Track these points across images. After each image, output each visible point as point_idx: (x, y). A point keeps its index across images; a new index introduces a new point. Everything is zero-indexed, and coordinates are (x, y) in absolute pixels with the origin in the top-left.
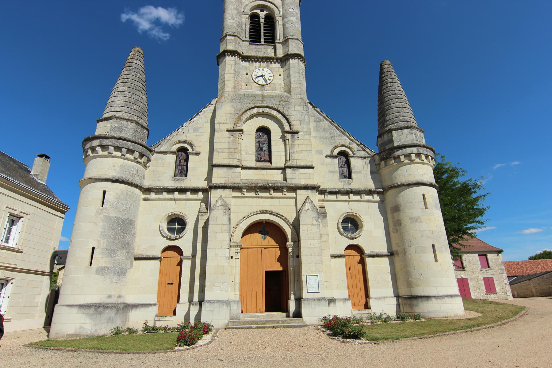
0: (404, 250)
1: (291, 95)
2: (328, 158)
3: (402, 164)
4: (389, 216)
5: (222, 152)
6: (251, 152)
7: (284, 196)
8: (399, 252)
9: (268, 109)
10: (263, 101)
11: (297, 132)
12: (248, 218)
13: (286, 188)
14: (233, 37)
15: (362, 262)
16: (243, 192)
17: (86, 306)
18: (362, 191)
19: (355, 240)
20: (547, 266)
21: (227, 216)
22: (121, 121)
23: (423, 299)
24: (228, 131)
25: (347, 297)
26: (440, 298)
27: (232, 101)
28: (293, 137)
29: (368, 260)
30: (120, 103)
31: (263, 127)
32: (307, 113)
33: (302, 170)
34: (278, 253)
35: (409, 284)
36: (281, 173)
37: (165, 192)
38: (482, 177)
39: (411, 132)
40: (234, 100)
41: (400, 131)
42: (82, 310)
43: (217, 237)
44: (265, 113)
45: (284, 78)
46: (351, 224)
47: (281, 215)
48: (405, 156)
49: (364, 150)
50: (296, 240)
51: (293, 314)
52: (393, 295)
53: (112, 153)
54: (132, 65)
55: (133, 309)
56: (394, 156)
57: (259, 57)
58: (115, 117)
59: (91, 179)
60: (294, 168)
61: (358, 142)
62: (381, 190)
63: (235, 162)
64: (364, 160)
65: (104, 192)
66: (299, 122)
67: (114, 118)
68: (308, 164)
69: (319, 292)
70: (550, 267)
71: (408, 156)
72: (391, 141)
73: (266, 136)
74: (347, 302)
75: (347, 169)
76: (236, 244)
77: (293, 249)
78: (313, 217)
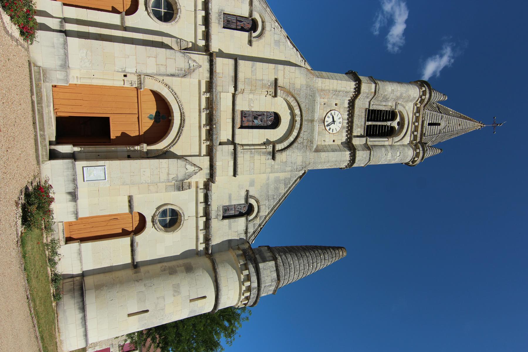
0: (140, 280)
2: (246, 193)
3: (239, 272)
4: (181, 262)
5: (252, 71)
6: (252, 105)
8: (138, 274)
9: (299, 126)
10: (308, 121)
11: (274, 158)
12: (175, 97)
13: (211, 144)
15: (125, 233)
21: (177, 72)
23: (81, 303)
26: (83, 323)
27: (308, 86)
28: (269, 153)
29: (127, 240)
33: (231, 163)
35: (98, 287)
36: (228, 140)
39: (274, 280)
40: (309, 89)
41: (275, 269)
43: (150, 58)
46: (170, 220)
47: (179, 138)
51: (54, 150)
52: (84, 270)
56: (248, 263)
57: (353, 119)
62: (210, 252)
63: (240, 86)
64: (243, 232)
68: (239, 170)
69: (84, 181)
72: (264, 260)
73: (270, 123)
74: (74, 215)
76: (142, 82)
77: (137, 152)
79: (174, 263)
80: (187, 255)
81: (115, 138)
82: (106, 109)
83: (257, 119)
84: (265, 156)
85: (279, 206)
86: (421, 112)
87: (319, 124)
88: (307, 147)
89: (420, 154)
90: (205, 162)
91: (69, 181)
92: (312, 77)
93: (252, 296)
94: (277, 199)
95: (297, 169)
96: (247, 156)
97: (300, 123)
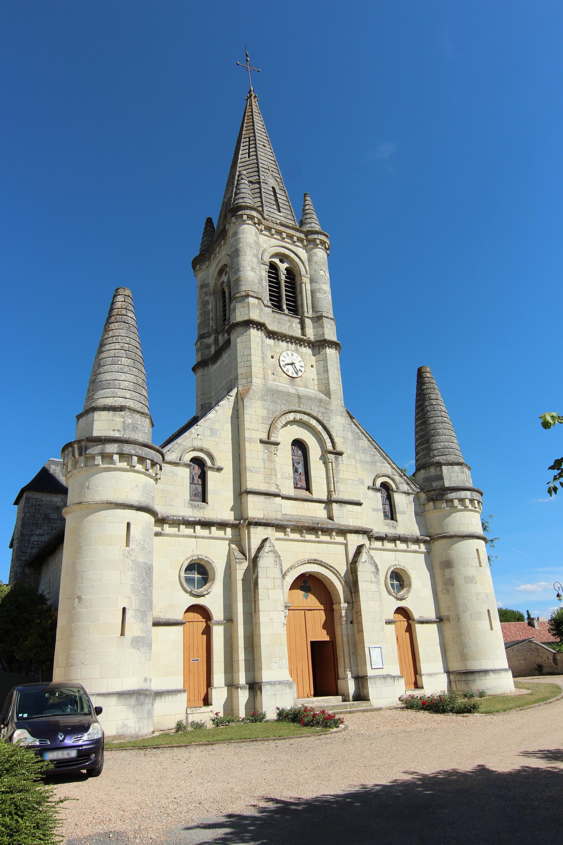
0: (458, 616)
1: (330, 399)
2: (371, 490)
3: (454, 509)
4: (437, 571)
5: (257, 472)
6: (287, 475)
7: (333, 540)
8: (450, 618)
9: (306, 416)
10: (299, 403)
11: (340, 454)
14: (257, 300)
15: (410, 630)
16: (288, 533)
17: (126, 694)
18: (410, 538)
19: (403, 601)
20: (510, 632)
21: (278, 566)
22: (134, 415)
23: (481, 674)
24: (262, 442)
25: (398, 673)
26: (497, 672)
27: (263, 399)
28: (336, 459)
29: (418, 628)
30: (127, 385)
31: (304, 444)
32: (350, 427)
33: (349, 507)
34: (324, 618)
35: (464, 657)
37: (183, 524)
38: (490, 516)
39: (462, 470)
40: (265, 398)
41: (450, 466)
42: (123, 701)
44: (301, 421)
45: (317, 370)
46: (397, 580)
47: (332, 567)
48: (459, 500)
49: (408, 484)
50: (349, 600)
51: (353, 697)
52: (443, 671)
53: (134, 467)
54: (128, 321)
55: (157, 698)
56: (446, 498)
57: (288, 336)
58: (129, 409)
59: (111, 503)
60: (341, 503)
61: (402, 472)
62: (428, 538)
63: (273, 490)
64: (408, 497)
65: (128, 525)
66: (342, 440)
67: (127, 409)
68: (355, 498)
69: (383, 668)
70: (513, 634)
71: (461, 500)
72: (440, 478)
73: (300, 452)
74: (400, 680)
75: (389, 506)
78: (372, 572)
79: (439, 580)
80: (430, 566)
81: (328, 636)
82: (302, 645)
83: (298, 469)
84: (340, 464)
85: (382, 450)
86: (271, 225)
87: (296, 385)
88: (326, 408)
89: (322, 239)
90: (351, 537)
91: (385, 683)
92: (252, 391)
93: (477, 498)
94: (374, 451)
95: (349, 424)
96: (340, 487)
97: (303, 415)
